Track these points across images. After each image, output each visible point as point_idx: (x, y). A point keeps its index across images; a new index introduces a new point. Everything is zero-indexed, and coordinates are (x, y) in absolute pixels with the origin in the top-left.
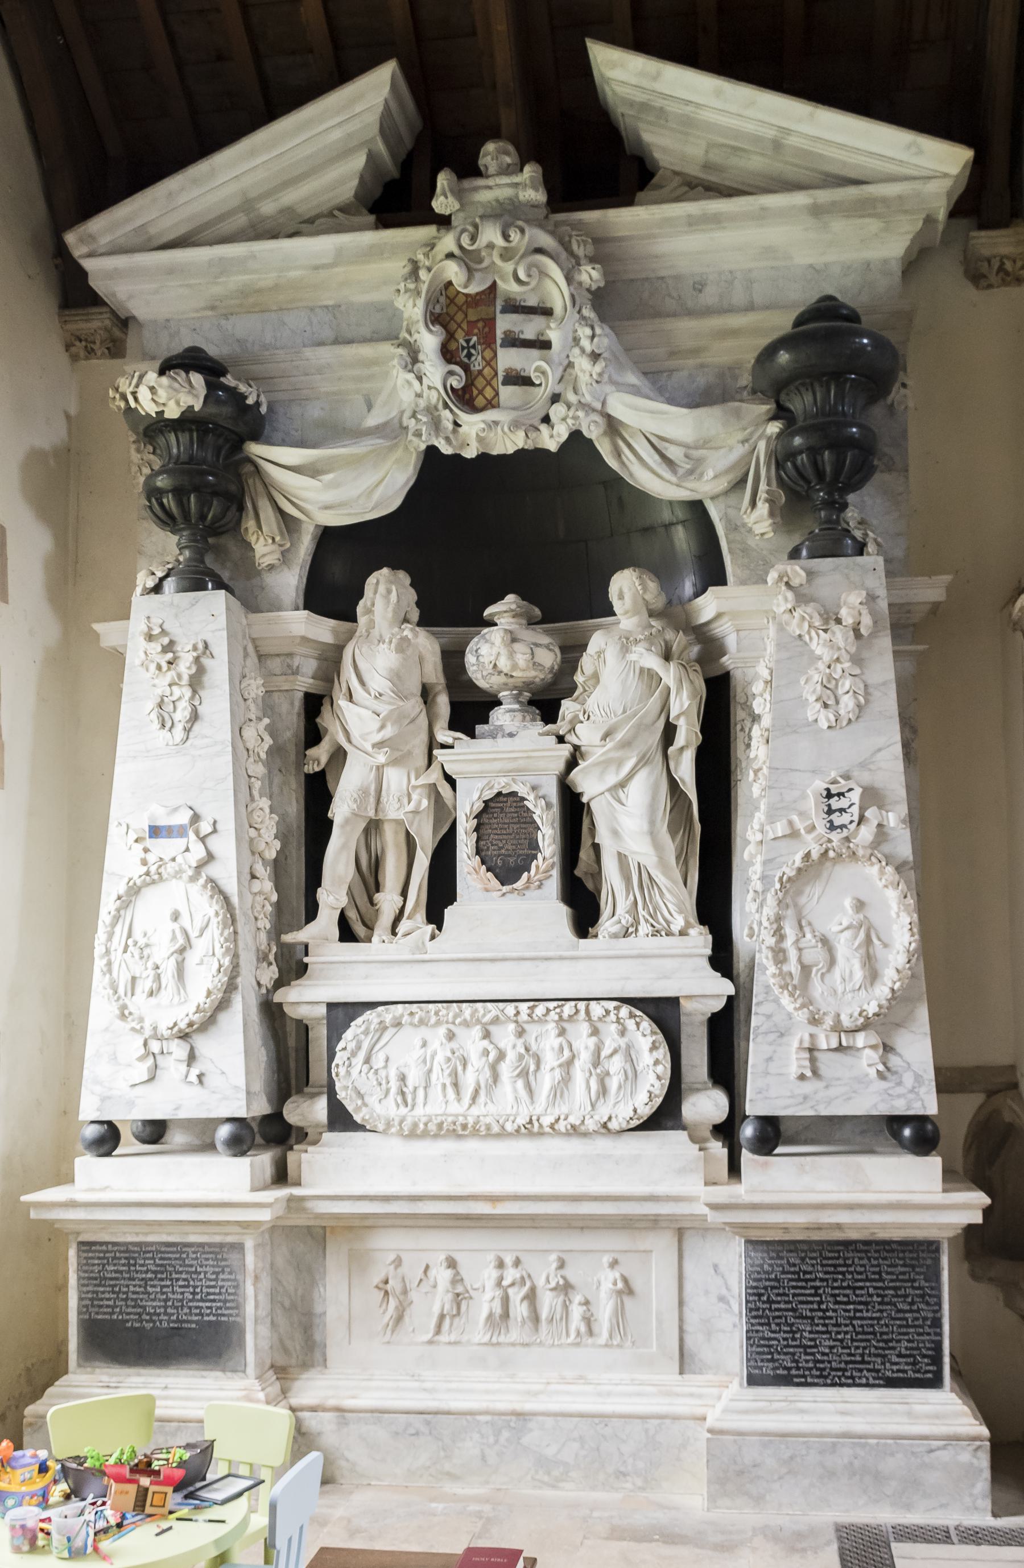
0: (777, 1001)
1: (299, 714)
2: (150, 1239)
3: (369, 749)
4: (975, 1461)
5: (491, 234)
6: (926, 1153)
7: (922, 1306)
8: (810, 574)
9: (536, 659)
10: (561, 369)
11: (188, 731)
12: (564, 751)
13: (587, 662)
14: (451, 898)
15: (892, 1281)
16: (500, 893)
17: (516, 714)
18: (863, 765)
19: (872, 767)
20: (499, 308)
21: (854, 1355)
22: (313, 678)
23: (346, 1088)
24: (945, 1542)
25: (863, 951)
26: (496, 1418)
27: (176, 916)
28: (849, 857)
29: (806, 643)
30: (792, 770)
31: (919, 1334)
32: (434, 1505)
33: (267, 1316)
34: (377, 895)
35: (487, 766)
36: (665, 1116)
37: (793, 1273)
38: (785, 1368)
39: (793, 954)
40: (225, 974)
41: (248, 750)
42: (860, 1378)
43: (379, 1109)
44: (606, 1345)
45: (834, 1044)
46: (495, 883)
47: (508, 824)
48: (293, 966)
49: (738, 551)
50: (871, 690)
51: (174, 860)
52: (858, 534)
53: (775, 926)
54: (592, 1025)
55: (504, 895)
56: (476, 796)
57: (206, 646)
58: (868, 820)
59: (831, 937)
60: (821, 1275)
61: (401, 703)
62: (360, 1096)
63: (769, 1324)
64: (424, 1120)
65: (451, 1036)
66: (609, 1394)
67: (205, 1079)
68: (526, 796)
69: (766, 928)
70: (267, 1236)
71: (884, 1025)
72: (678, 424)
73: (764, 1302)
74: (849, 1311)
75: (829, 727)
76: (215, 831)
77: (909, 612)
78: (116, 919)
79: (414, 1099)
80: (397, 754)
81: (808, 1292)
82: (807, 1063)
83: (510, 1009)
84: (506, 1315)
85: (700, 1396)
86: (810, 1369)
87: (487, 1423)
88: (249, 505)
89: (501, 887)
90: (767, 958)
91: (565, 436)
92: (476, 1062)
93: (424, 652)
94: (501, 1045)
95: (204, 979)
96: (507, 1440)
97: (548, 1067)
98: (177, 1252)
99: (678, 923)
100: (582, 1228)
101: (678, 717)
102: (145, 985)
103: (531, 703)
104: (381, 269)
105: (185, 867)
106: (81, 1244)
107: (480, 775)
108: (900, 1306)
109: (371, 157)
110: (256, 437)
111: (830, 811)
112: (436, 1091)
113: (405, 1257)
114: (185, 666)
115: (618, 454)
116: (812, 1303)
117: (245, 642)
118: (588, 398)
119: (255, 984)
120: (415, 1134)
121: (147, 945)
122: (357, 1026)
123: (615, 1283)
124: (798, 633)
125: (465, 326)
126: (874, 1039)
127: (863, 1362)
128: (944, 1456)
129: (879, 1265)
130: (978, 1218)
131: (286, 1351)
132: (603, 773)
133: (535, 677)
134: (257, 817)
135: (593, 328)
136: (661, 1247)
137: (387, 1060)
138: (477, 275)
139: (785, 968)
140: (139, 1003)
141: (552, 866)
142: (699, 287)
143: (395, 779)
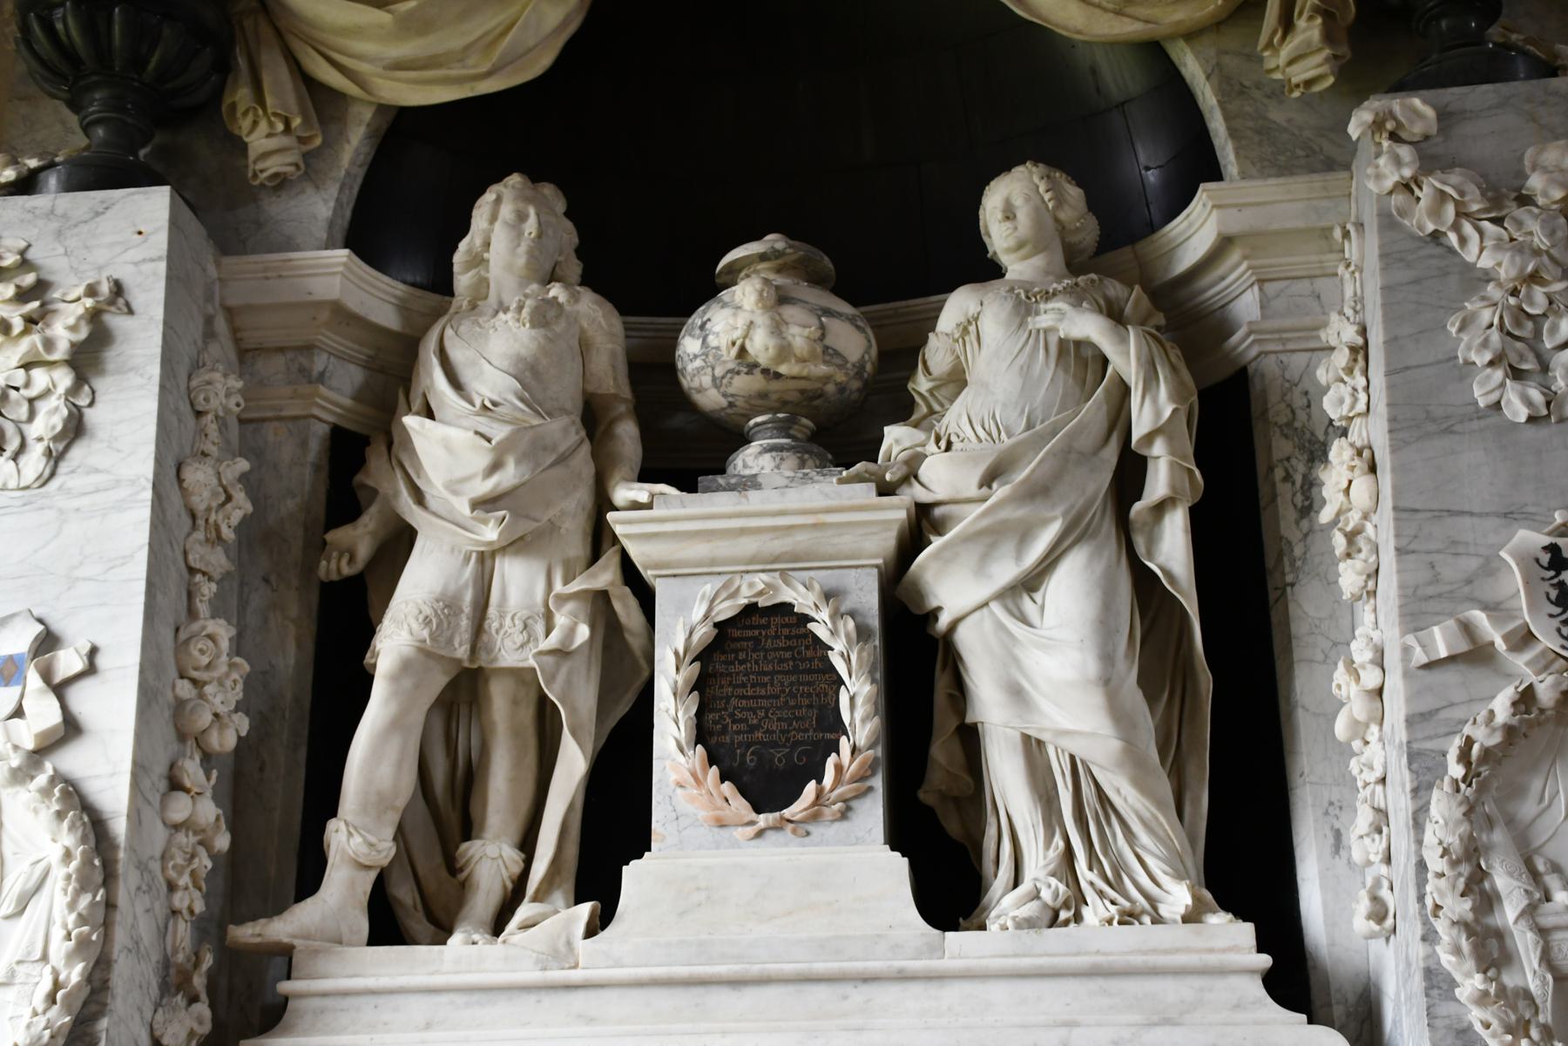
1: (317, 468)
9: (828, 341)
11: (55, 459)
13: (938, 353)
14: (638, 842)
16: (751, 830)
17: (785, 454)
22: (353, 398)
29: (1451, 250)
30: (1452, 513)
34: (465, 846)
35: (723, 548)
39: (1525, 943)
40: (67, 1007)
41: (193, 517)
46: (740, 806)
47: (772, 673)
49: (1249, 133)
53: (1465, 869)
55: (760, 834)
56: (698, 612)
57: (118, 289)
61: (536, 421)
68: (813, 614)
69: (1441, 875)
75: (1532, 419)
76: (91, 670)
80: (526, 527)
88: (242, 62)
89: (753, 816)
90: (1457, 951)
93: (591, 332)
101: (1149, 438)
114: (64, 330)
117: (210, 310)
124: (1430, 227)
132: (985, 558)
133: (827, 379)
134: (199, 654)
139: (1510, 980)
141: (872, 768)
143: (519, 582)
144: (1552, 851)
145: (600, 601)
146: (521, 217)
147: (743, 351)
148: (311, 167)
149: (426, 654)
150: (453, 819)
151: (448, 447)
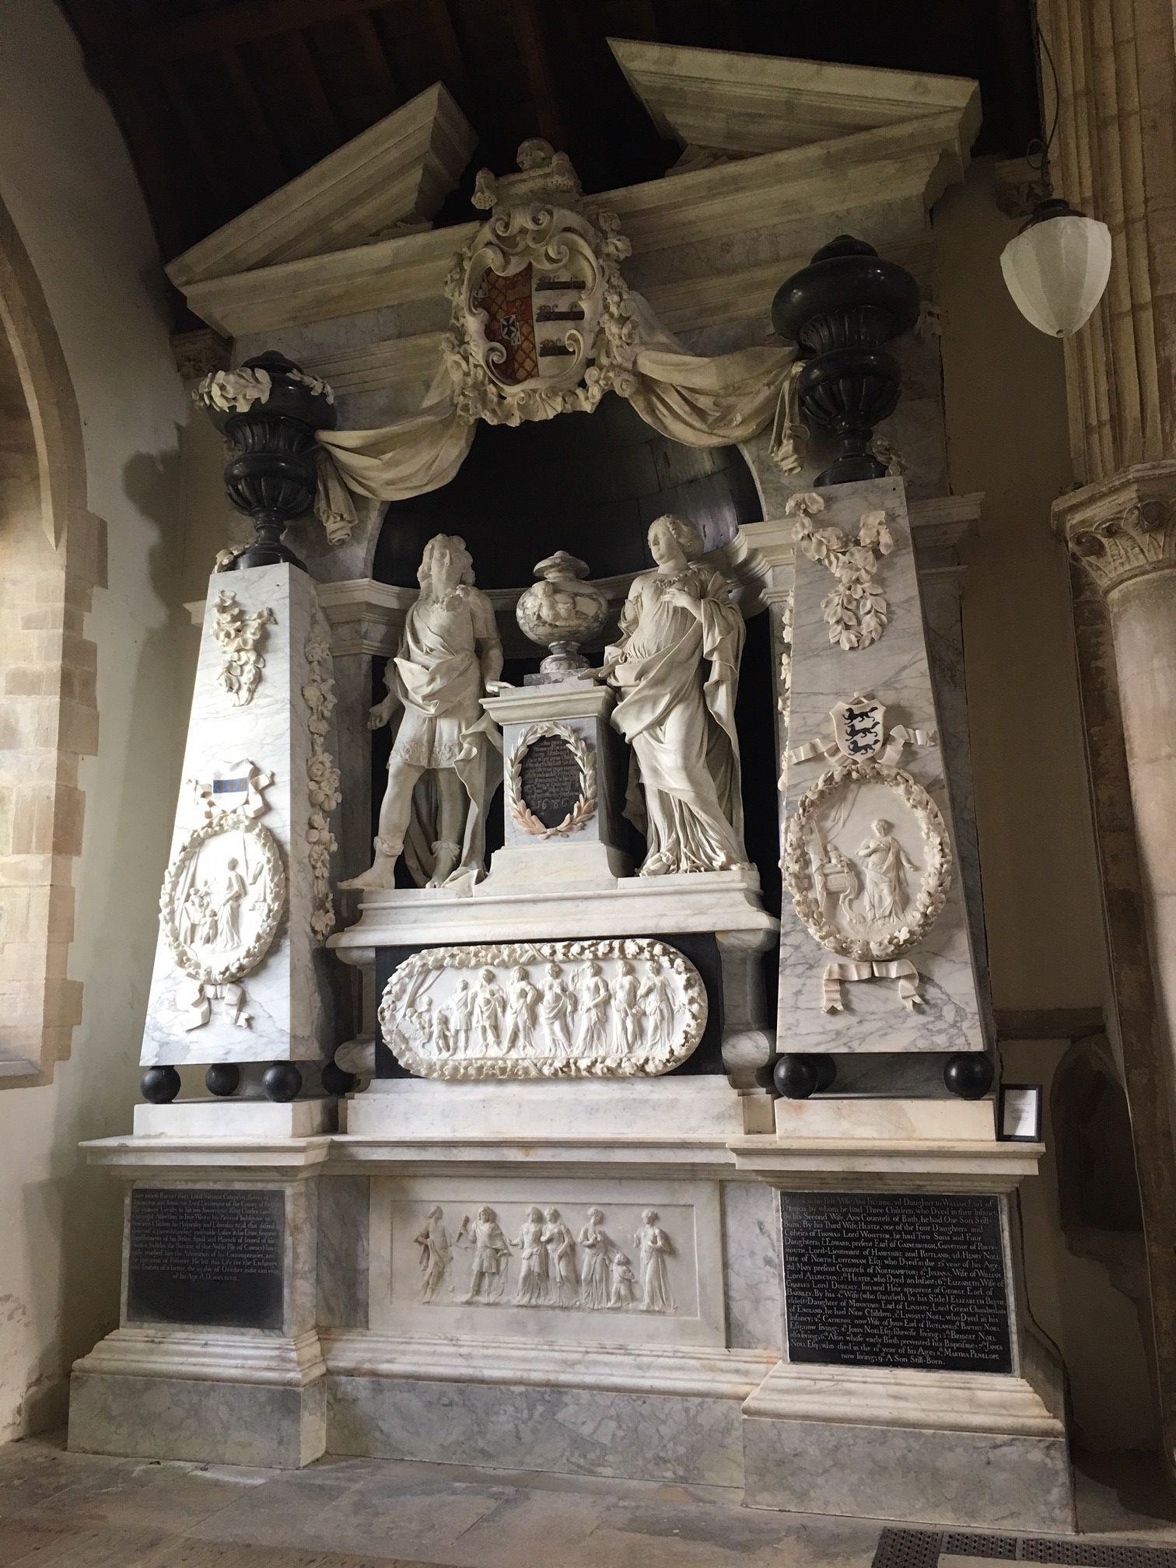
0: (805, 931)
1: (366, 677)
2: (198, 1186)
3: (420, 701)
4: (1048, 1461)
5: (522, 220)
6: (977, 1097)
7: (981, 1273)
8: (829, 500)
10: (593, 335)
11: (252, 692)
12: (601, 692)
13: (629, 610)
15: (945, 1242)
18: (887, 685)
19: (897, 685)
20: (534, 286)
21: (907, 1329)
23: (390, 1032)
24: (1008, 1558)
25: (892, 874)
26: (530, 1388)
27: (233, 865)
28: (874, 777)
31: (980, 1307)
32: (457, 1484)
33: (311, 1271)
35: (529, 712)
36: (702, 1059)
37: (834, 1230)
38: (831, 1342)
39: (818, 880)
40: (274, 918)
42: (916, 1356)
43: (422, 1054)
44: (647, 1311)
45: (866, 975)
46: (539, 825)
48: (349, 911)
50: (893, 608)
51: (234, 812)
52: (880, 458)
53: (798, 852)
54: (626, 964)
56: (520, 741)
57: (271, 612)
58: (894, 739)
59: (858, 862)
60: (865, 1234)
62: (406, 1040)
63: (811, 1289)
64: (464, 1063)
65: (490, 978)
66: (649, 1366)
67: (254, 1023)
70: (313, 1185)
71: (919, 952)
72: (702, 374)
73: (805, 1264)
74: (899, 1276)
75: (851, 648)
77: (945, 533)
78: (181, 869)
79: (456, 1042)
80: (448, 706)
81: (852, 1253)
82: (837, 996)
83: (546, 949)
84: (545, 1274)
85: (746, 1373)
86: (859, 1344)
87: (520, 1394)
91: (598, 397)
92: (515, 1003)
94: (539, 986)
95: (255, 922)
96: (541, 1415)
97: (585, 1009)
98: (222, 1201)
99: (720, 858)
100: (620, 1179)
101: (711, 652)
102: (203, 931)
103: (580, 652)
104: (434, 263)
105: (243, 818)
106: (136, 1191)
107: (522, 721)
108: (957, 1272)
109: (427, 170)
110: (331, 426)
111: (854, 732)
112: (476, 1035)
113: (446, 1209)
114: (250, 635)
115: (652, 410)
116: (857, 1266)
118: (619, 360)
119: (309, 929)
120: (457, 1078)
121: (207, 894)
122: (402, 968)
123: (654, 1241)
125: (504, 306)
126: (909, 968)
127: (917, 1338)
128: (1012, 1453)
129: (929, 1224)
130: (1031, 1168)
131: (331, 1310)
132: (640, 712)
135: (620, 295)
136: (702, 1200)
137: (430, 1003)
138: (514, 260)
140: (198, 950)
141: (595, 806)
142: (726, 247)
143: (447, 729)
144: (836, 842)
145: (482, 735)
146: (443, 556)
147: (539, 617)
148: (356, 533)
149: (408, 765)
150: (431, 831)
151: (411, 671)
